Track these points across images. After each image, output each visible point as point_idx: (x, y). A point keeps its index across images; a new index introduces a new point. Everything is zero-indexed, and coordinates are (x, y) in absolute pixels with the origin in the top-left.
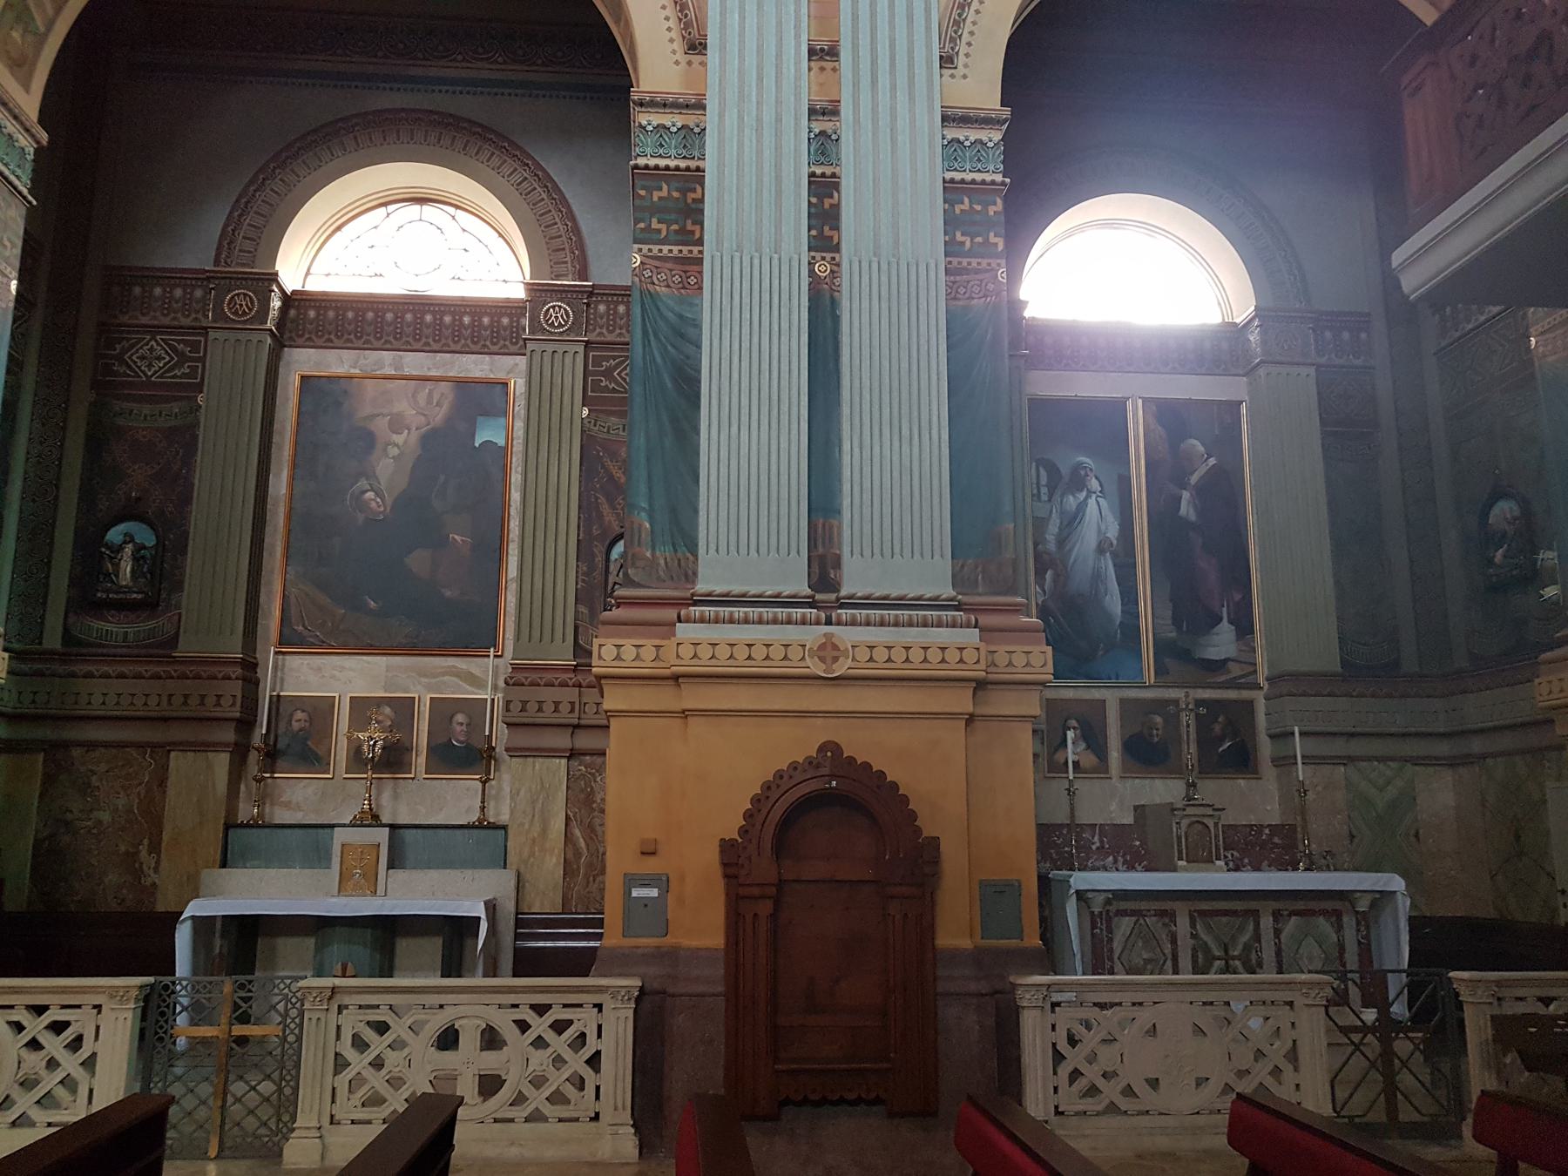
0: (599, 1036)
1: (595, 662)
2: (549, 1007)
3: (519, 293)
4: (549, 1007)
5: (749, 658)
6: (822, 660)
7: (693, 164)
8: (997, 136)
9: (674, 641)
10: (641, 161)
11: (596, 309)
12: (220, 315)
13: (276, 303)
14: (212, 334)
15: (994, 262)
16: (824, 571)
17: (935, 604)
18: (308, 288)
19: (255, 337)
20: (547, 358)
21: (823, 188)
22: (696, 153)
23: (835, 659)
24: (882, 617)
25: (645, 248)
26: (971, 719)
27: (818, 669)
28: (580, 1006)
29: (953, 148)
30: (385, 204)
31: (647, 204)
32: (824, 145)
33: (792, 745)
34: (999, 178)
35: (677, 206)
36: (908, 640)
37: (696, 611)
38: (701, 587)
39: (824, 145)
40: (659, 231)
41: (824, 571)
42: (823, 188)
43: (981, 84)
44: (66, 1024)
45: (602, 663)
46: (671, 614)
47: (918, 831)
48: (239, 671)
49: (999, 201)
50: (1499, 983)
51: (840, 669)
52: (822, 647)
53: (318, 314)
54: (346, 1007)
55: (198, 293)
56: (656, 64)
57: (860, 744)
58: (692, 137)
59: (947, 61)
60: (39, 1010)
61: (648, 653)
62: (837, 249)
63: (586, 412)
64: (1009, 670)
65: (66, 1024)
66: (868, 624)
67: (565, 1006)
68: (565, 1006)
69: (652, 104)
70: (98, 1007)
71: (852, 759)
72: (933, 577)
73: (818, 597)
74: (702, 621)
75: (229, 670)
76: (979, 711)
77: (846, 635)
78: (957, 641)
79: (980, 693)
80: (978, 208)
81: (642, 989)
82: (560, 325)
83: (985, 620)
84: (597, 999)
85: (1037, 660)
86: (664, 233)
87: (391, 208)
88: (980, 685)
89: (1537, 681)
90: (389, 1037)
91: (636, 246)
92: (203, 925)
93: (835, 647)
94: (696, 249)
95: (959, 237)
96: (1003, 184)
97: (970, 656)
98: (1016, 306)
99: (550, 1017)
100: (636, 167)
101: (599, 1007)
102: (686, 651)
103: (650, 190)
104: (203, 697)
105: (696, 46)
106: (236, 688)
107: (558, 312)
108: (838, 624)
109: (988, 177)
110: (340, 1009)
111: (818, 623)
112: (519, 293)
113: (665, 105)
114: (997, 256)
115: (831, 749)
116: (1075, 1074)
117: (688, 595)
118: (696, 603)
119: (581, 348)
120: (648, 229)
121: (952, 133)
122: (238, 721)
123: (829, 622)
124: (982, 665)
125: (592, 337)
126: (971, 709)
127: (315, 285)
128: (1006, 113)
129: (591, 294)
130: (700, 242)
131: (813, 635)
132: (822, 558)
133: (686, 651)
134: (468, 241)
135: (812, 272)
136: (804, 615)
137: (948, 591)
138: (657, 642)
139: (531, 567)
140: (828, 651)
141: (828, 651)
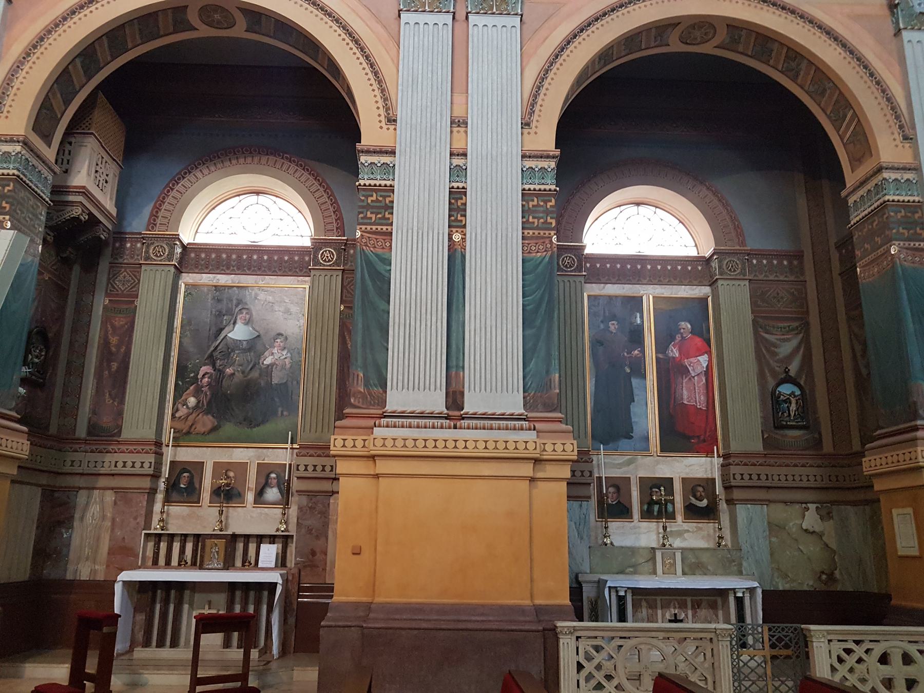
1: (332, 447)
3: (307, 243)
7: (388, 183)
8: (553, 164)
9: (372, 437)
10: (362, 182)
11: (348, 252)
12: (148, 258)
13: (179, 250)
14: (143, 267)
16: (455, 399)
17: (512, 417)
18: (197, 241)
19: (168, 268)
21: (457, 197)
25: (363, 227)
26: (532, 480)
30: (239, 195)
31: (365, 204)
32: (457, 172)
35: (382, 204)
37: (384, 421)
38: (389, 408)
39: (457, 172)
40: (371, 218)
41: (455, 399)
42: (457, 197)
43: (545, 138)
46: (370, 422)
48: (153, 448)
49: (553, 200)
50: (829, 632)
53: (206, 256)
54: (580, 637)
55: (139, 245)
56: (371, 131)
58: (389, 169)
59: (526, 125)
61: (359, 444)
62: (464, 226)
63: (342, 308)
67: (871, 641)
68: (871, 641)
72: (514, 404)
75: (147, 448)
78: (525, 439)
79: (538, 467)
80: (542, 204)
82: (329, 261)
84: (709, 636)
85: (569, 448)
86: (373, 219)
87: (242, 197)
88: (537, 461)
89: (864, 460)
91: (358, 227)
92: (126, 584)
94: (389, 228)
95: (531, 219)
96: (555, 190)
100: (360, 185)
103: (367, 197)
104: (142, 463)
106: (151, 458)
107: (329, 253)
109: (547, 187)
110: (578, 638)
111: (450, 428)
112: (307, 243)
114: (552, 229)
116: (589, 677)
117: (380, 412)
118: (385, 417)
119: (340, 273)
120: (365, 217)
121: (529, 163)
122: (152, 476)
123: (455, 427)
124: (538, 450)
125: (347, 267)
126: (531, 474)
127: (201, 239)
128: (558, 152)
129: (346, 244)
130: (391, 224)
132: (454, 392)
133: (379, 443)
134: (282, 215)
135: (450, 238)
137: (519, 410)
138: (365, 438)
139: (314, 391)
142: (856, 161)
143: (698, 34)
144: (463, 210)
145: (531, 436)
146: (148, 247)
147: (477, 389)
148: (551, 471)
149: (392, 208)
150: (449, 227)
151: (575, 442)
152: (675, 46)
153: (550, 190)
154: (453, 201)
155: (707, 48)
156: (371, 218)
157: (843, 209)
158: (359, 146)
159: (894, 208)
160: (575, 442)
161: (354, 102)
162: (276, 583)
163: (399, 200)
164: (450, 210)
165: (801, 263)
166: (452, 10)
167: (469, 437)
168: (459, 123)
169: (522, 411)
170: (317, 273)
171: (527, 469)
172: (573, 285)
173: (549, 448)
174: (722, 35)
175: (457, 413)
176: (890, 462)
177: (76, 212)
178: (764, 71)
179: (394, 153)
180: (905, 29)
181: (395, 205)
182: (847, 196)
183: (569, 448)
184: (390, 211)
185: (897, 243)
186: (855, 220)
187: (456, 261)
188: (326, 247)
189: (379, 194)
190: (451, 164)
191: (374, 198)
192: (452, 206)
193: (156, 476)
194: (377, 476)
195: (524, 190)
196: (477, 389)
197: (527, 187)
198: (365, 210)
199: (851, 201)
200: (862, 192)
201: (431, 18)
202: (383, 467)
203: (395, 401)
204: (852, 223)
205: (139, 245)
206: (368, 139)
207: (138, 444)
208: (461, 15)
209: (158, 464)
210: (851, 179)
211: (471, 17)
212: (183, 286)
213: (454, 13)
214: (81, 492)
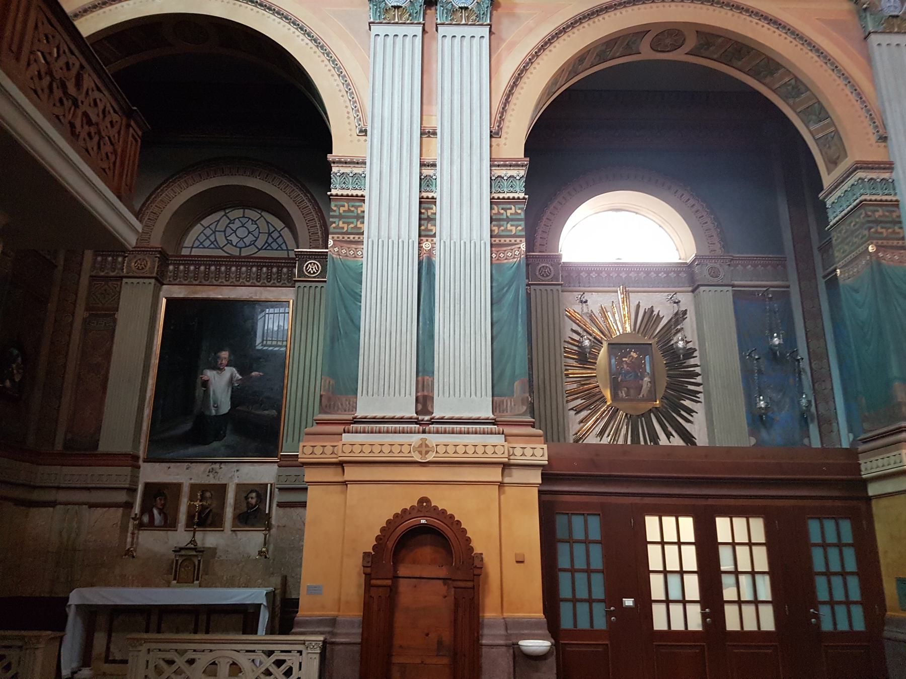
0: (300, 669)
2: (186, 651)
4: (186, 651)
5: (465, 452)
6: (420, 453)
9: (340, 444)
10: (334, 192)
15: (518, 240)
16: (424, 402)
17: (410, 421)
20: (318, 290)
22: (892, 192)
23: (427, 452)
24: (372, 428)
26: (501, 485)
27: (417, 458)
28: (290, 652)
29: (494, 181)
33: (406, 499)
34: (522, 195)
36: (466, 441)
39: (425, 182)
41: (424, 402)
42: (426, 203)
43: (514, 144)
44: (284, 661)
45: (304, 456)
46: (340, 428)
47: (472, 549)
51: (430, 457)
52: (421, 446)
56: (343, 144)
57: (442, 500)
58: (359, 179)
60: (270, 653)
64: (390, 455)
65: (284, 661)
66: (380, 432)
67: (282, 651)
68: (282, 651)
69: (340, 162)
70: (300, 652)
71: (436, 508)
73: (420, 418)
74: (437, 432)
76: (507, 480)
77: (433, 439)
78: (493, 444)
79: (507, 471)
81: (324, 642)
82: (314, 273)
83: (508, 430)
85: (538, 452)
90: (174, 667)
93: (427, 446)
96: (524, 198)
97: (499, 450)
98: (559, 257)
99: (274, 658)
100: (331, 195)
101: (300, 652)
102: (347, 449)
105: (884, 139)
108: (430, 433)
109: (516, 195)
113: (346, 163)
115: (424, 500)
117: (350, 417)
120: (876, 232)
123: (424, 432)
124: (506, 455)
126: (500, 479)
130: (362, 233)
131: (416, 439)
135: (420, 248)
136: (372, 428)
137: (487, 413)
140: (424, 448)
141: (424, 448)
142: (833, 163)
143: (668, 41)
144: (431, 219)
145: (499, 440)
146: (130, 261)
147: (447, 394)
148: (517, 476)
149: (363, 217)
150: (420, 236)
151: (545, 446)
152: (646, 53)
153: (519, 198)
154: (423, 211)
155: (678, 56)
156: (343, 228)
157: (821, 210)
158: (330, 157)
159: (871, 208)
160: (545, 446)
161: (326, 113)
162: (259, 606)
163: (370, 209)
164: (420, 219)
165: (785, 267)
166: (421, 20)
167: (440, 443)
168: (427, 133)
169: (492, 416)
170: (302, 284)
171: (495, 474)
172: (544, 293)
173: (518, 452)
174: (691, 42)
175: (427, 418)
176: (874, 466)
177: (621, 324)
178: (731, 74)
179: (365, 163)
180: (875, 32)
181: (438, 216)
182: (825, 198)
183: (538, 452)
184: (433, 222)
185: (875, 241)
186: (834, 221)
187: (426, 270)
188: (315, 259)
189: (501, 206)
190: (421, 174)
191: (513, 211)
192: (423, 216)
193: (132, 491)
194: (345, 483)
195: (421, 198)
196: (447, 394)
197: (496, 196)
198: (355, 220)
199: (829, 203)
200: (838, 193)
201: (401, 30)
202: (351, 473)
203: (536, 477)
204: (831, 224)
205: (120, 259)
206: (339, 150)
207: (112, 459)
208: (430, 28)
209: (135, 479)
210: (827, 180)
211: (440, 28)
212: (164, 301)
213: (424, 24)
214: (58, 507)
